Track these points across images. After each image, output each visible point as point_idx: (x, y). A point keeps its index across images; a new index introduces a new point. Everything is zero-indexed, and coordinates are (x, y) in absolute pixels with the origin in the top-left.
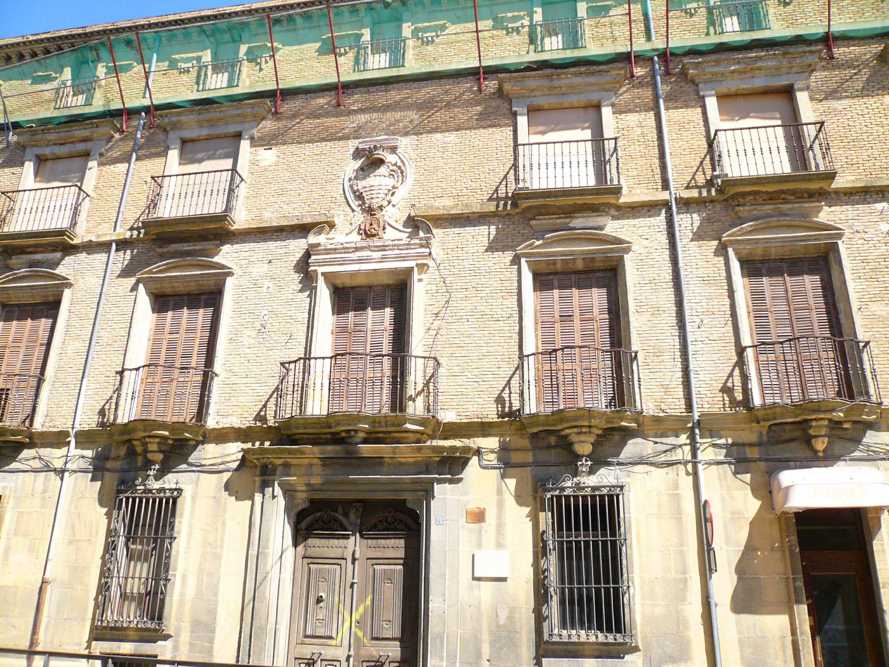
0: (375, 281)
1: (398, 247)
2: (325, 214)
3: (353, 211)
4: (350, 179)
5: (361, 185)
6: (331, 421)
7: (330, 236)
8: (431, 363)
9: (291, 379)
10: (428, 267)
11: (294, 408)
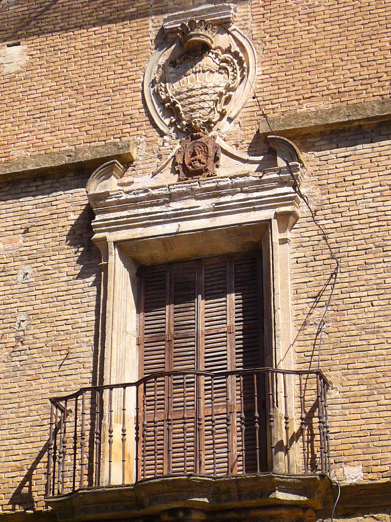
0: (178, 252)
1: (242, 188)
2: (115, 144)
3: (162, 134)
4: (153, 83)
5: (171, 89)
6: (143, 494)
7: (126, 180)
8: (313, 383)
9: (70, 427)
10: (297, 218)
11: (78, 478)
